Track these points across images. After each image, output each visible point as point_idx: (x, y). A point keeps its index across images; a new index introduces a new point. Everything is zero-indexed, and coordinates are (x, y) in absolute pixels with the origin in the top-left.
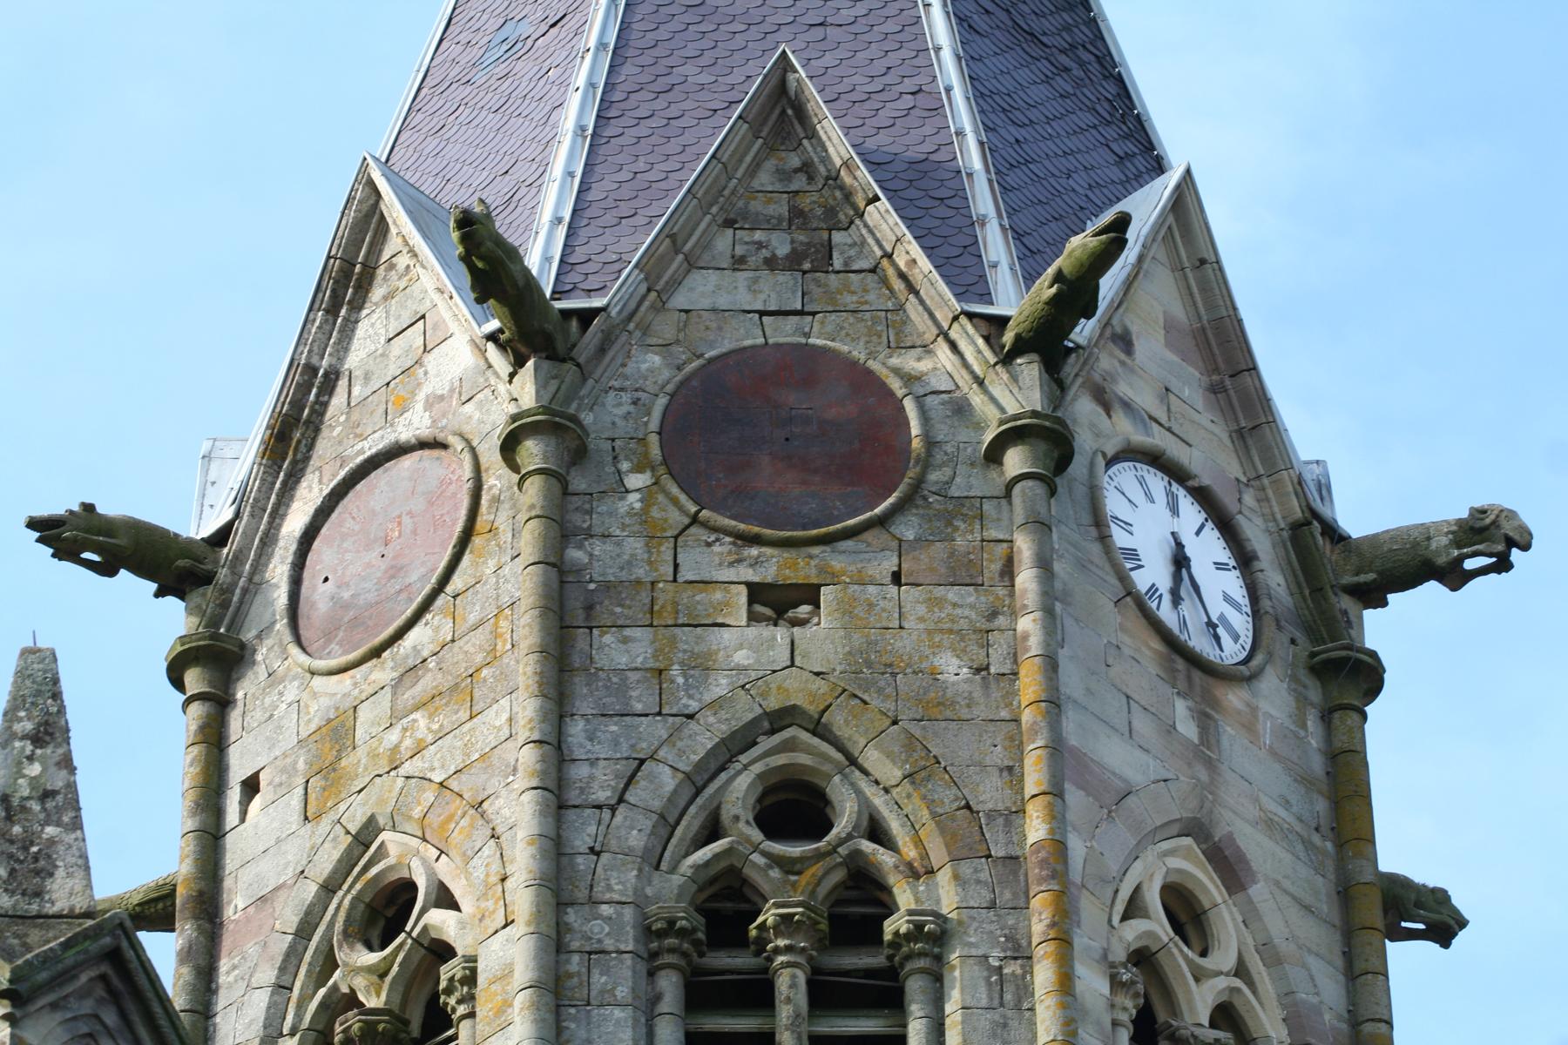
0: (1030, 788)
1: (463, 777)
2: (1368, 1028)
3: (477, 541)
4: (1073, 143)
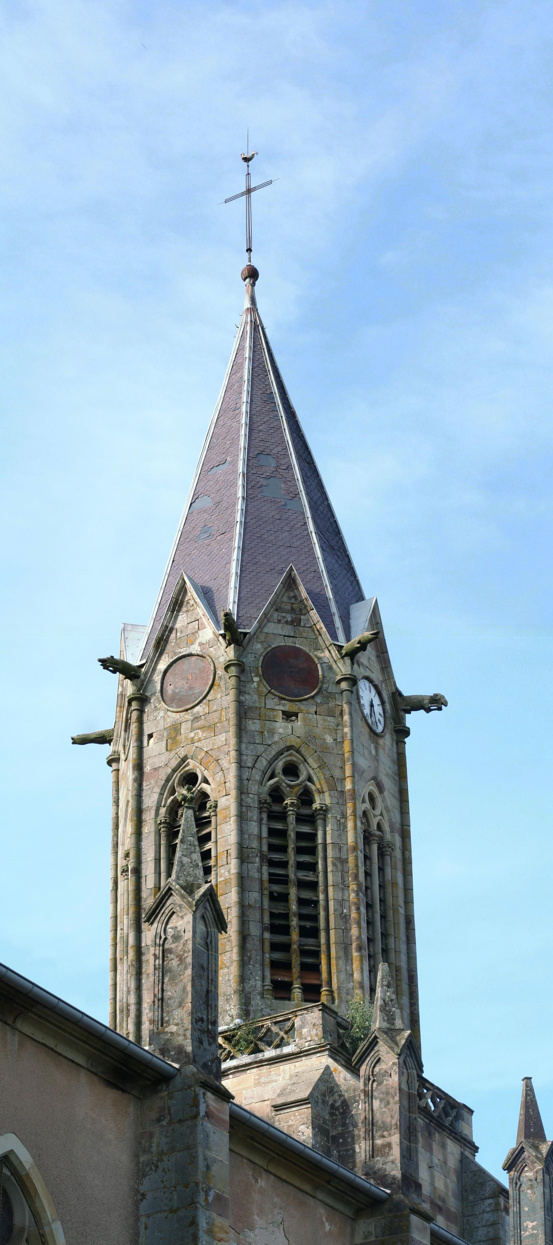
1: (213, 752)
3: (215, 687)
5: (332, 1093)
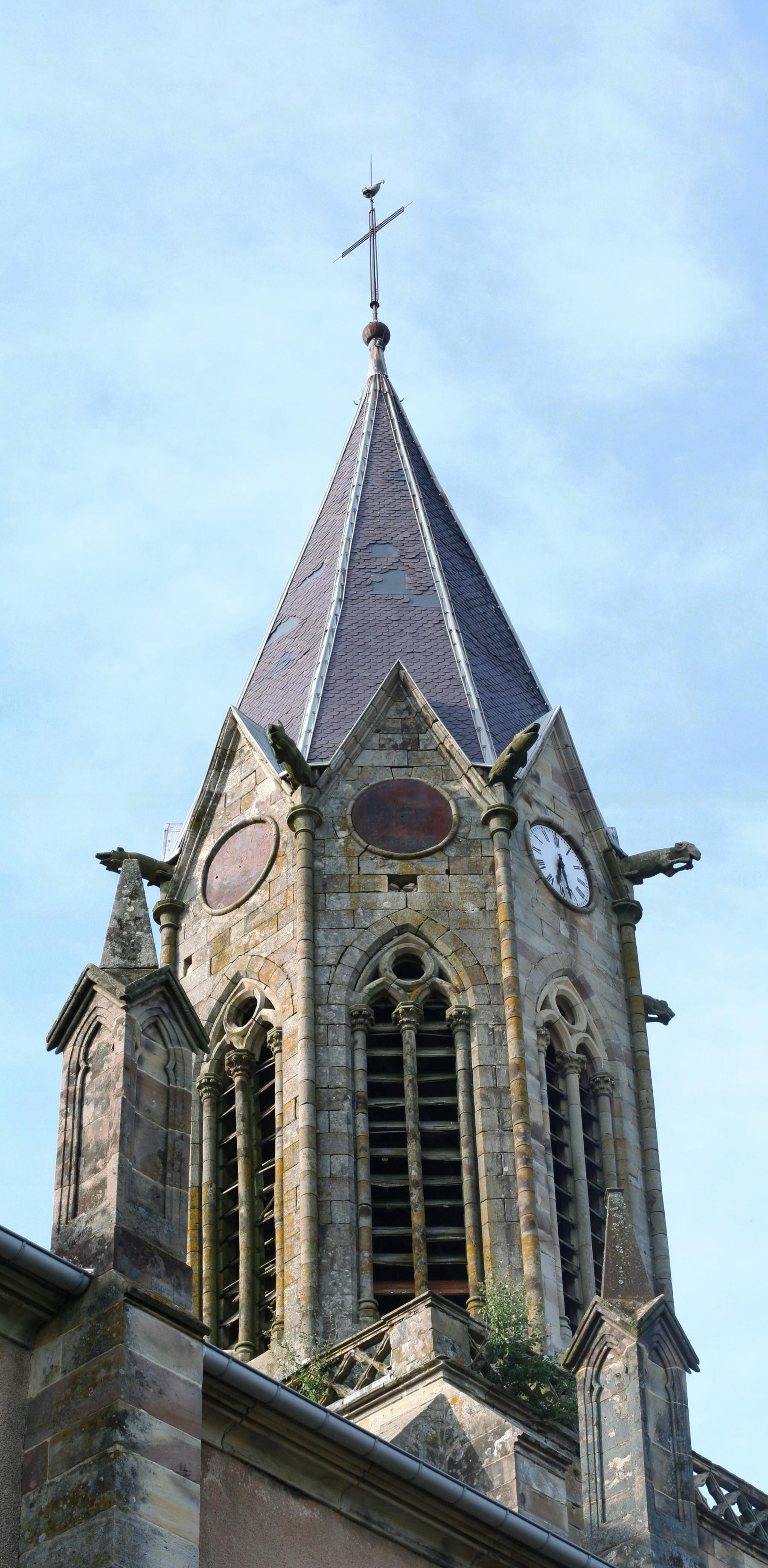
0: (504, 955)
1: (275, 955)
2: (639, 1053)
3: (278, 860)
4: (514, 699)
5: (450, 1441)
